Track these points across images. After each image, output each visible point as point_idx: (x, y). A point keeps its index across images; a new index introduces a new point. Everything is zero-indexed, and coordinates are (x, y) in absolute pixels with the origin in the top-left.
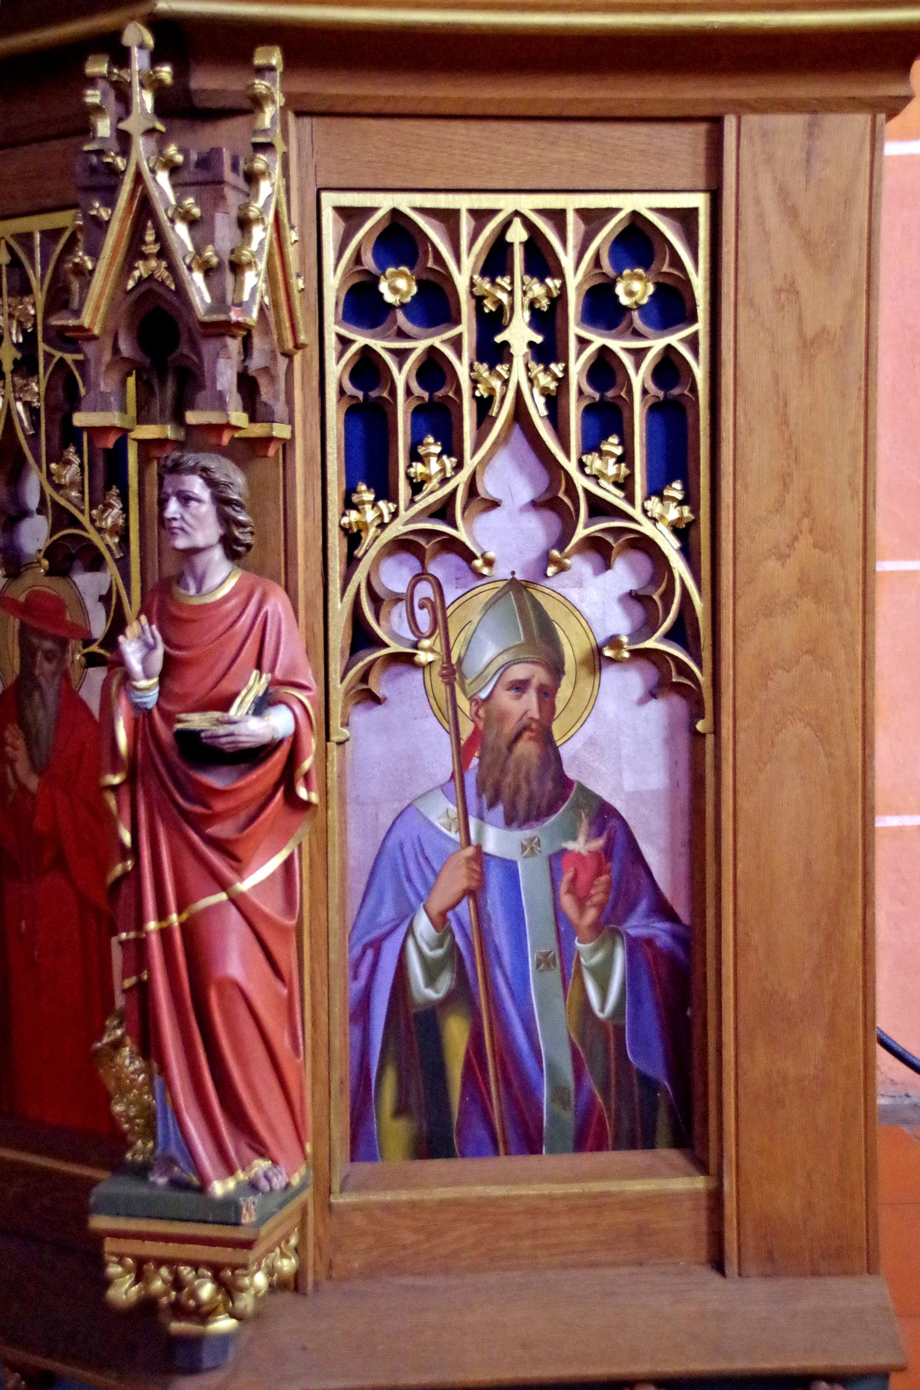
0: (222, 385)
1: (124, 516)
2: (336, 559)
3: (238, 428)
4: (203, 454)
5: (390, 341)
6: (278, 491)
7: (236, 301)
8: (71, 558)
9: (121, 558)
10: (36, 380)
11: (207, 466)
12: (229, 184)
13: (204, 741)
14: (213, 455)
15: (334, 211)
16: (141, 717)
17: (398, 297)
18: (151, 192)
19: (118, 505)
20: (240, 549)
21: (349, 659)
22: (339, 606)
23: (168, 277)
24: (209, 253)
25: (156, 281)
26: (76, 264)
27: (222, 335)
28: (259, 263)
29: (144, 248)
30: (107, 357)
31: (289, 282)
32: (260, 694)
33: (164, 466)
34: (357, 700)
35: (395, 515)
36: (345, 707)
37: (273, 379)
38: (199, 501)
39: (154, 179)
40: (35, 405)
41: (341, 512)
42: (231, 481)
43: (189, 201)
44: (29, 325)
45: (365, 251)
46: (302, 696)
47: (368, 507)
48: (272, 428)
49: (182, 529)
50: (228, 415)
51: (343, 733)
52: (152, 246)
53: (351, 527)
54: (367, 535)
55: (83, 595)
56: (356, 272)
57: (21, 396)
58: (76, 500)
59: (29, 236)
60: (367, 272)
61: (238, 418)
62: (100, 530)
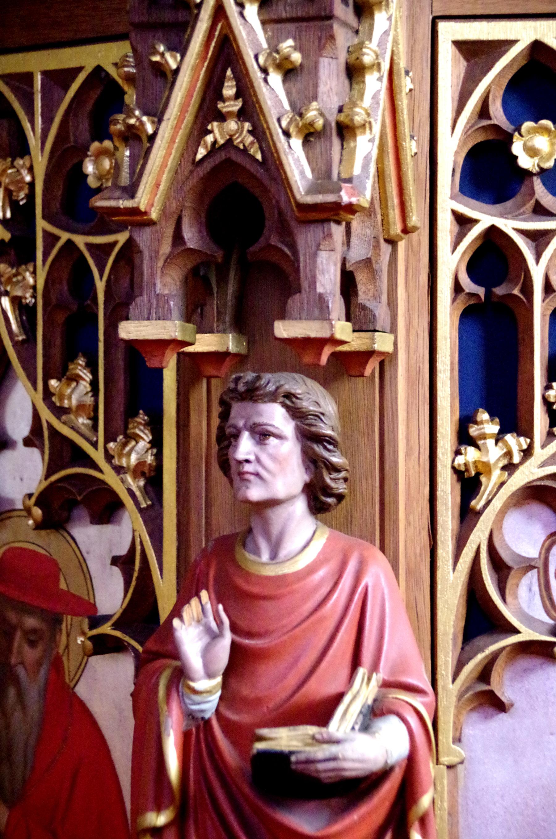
0: (323, 285)
1: (155, 451)
2: (447, 512)
3: (342, 342)
4: (285, 374)
5: (525, 220)
6: (373, 421)
7: (344, 176)
8: (72, 505)
9: (148, 506)
10: (31, 269)
11: (293, 391)
12: (337, 18)
13: (293, 767)
14: (296, 376)
15: (453, 46)
16: (194, 729)
17: (536, 160)
18: (236, 32)
19: (146, 437)
20: (330, 500)
21: (462, 649)
22: (451, 576)
23: (252, 143)
24: (311, 114)
25: (237, 148)
26: (130, 127)
27: (325, 221)
28: (373, 123)
29: (220, 105)
30: (166, 248)
31: (402, 144)
32: (370, 702)
33: (235, 390)
34: (473, 705)
35: (527, 453)
36: (457, 716)
37: (373, 274)
38: (279, 437)
39: (242, 15)
40: (28, 301)
41: (454, 449)
42: (321, 410)
43: (287, 45)
44: (22, 195)
45: (494, 100)
46: (417, 701)
47: (490, 442)
48: (373, 339)
49: (257, 475)
50: (332, 326)
51: (455, 753)
52: (232, 103)
53: (467, 470)
54: (489, 479)
55: (85, 555)
56: (480, 128)
57: (8, 288)
58: (83, 429)
59: (28, 77)
60: (496, 128)
61: (343, 330)
62: (119, 470)
